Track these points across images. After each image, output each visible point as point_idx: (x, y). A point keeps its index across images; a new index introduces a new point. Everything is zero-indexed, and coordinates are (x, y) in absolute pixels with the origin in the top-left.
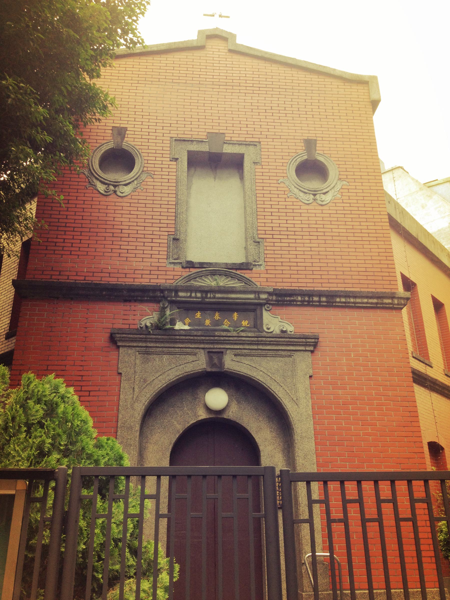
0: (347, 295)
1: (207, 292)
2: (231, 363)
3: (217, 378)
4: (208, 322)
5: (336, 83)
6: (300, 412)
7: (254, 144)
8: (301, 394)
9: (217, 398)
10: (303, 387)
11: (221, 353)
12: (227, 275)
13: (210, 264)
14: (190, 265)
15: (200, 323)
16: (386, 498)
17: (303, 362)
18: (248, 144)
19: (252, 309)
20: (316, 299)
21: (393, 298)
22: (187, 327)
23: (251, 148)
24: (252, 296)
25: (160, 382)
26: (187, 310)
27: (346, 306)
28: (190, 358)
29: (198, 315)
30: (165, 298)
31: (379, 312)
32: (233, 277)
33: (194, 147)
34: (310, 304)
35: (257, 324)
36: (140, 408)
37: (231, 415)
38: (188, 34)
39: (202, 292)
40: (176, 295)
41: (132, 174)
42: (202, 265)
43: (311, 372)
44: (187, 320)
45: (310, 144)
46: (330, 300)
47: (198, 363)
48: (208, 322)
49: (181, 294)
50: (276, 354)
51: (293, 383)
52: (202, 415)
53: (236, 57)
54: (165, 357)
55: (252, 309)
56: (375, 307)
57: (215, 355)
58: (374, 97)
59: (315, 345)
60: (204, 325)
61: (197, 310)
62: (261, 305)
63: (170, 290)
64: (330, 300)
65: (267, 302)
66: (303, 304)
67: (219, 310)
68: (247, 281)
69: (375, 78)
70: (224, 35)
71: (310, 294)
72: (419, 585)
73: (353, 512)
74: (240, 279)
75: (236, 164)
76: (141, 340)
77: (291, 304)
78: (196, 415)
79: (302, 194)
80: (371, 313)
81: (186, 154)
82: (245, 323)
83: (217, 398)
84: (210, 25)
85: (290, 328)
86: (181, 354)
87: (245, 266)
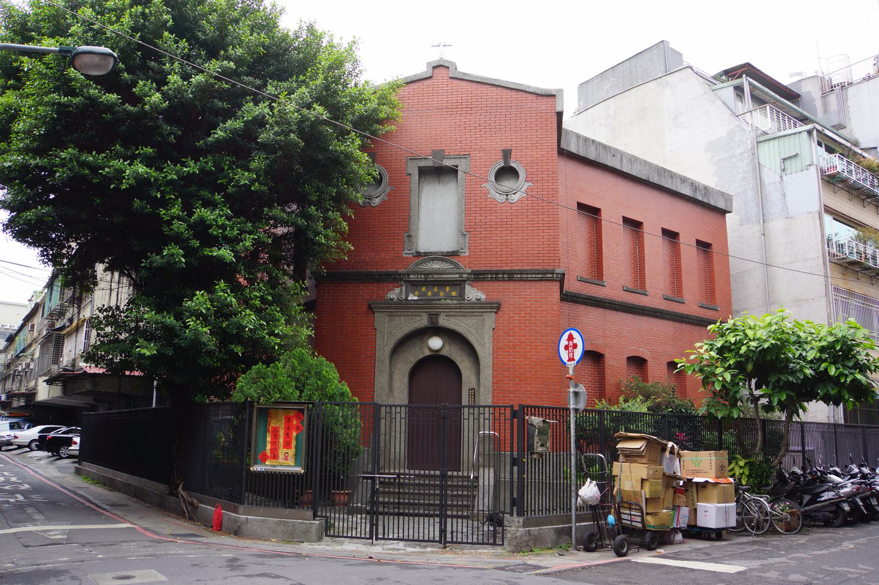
0: (521, 272)
1: (428, 274)
2: (444, 321)
3: (436, 330)
4: (430, 294)
5: (531, 97)
6: (485, 351)
7: (464, 157)
8: (486, 341)
9: (436, 343)
10: (488, 336)
11: (437, 315)
12: (443, 260)
13: (431, 253)
14: (419, 254)
15: (425, 294)
16: (382, 444)
17: (490, 320)
18: (460, 157)
19: (458, 284)
20: (500, 276)
21: (553, 273)
22: (416, 298)
23: (463, 160)
24: (457, 276)
25: (400, 333)
26: (417, 286)
27: (521, 280)
28: (418, 318)
29: (424, 289)
30: (401, 280)
31: (544, 283)
32: (447, 261)
33: (422, 164)
34: (497, 279)
35: (462, 295)
36: (388, 350)
37: (444, 353)
38: (420, 68)
39: (424, 274)
40: (409, 277)
41: (380, 189)
42: (426, 254)
43: (494, 326)
44: (417, 293)
45: (507, 154)
46: (510, 276)
47: (422, 321)
48: (430, 294)
49: (411, 276)
50: (472, 314)
51: (481, 332)
52: (427, 353)
53: (455, 82)
54: (403, 318)
55: (458, 284)
56: (541, 280)
57: (433, 317)
58: (558, 109)
59: (498, 308)
60: (426, 295)
61: (423, 285)
62: (465, 281)
63: (404, 275)
64: (510, 276)
65: (468, 279)
66: (492, 280)
67: (437, 285)
68: (456, 265)
69: (561, 91)
70: (446, 65)
71: (497, 273)
72: (800, 443)
73: (502, 418)
74: (451, 263)
75: (453, 171)
76: (387, 308)
77: (484, 280)
78: (423, 353)
79: (498, 195)
80: (538, 284)
81: (417, 169)
82: (454, 294)
83: (436, 343)
84: (434, 57)
85: (483, 297)
86: (412, 316)
87: (454, 254)
